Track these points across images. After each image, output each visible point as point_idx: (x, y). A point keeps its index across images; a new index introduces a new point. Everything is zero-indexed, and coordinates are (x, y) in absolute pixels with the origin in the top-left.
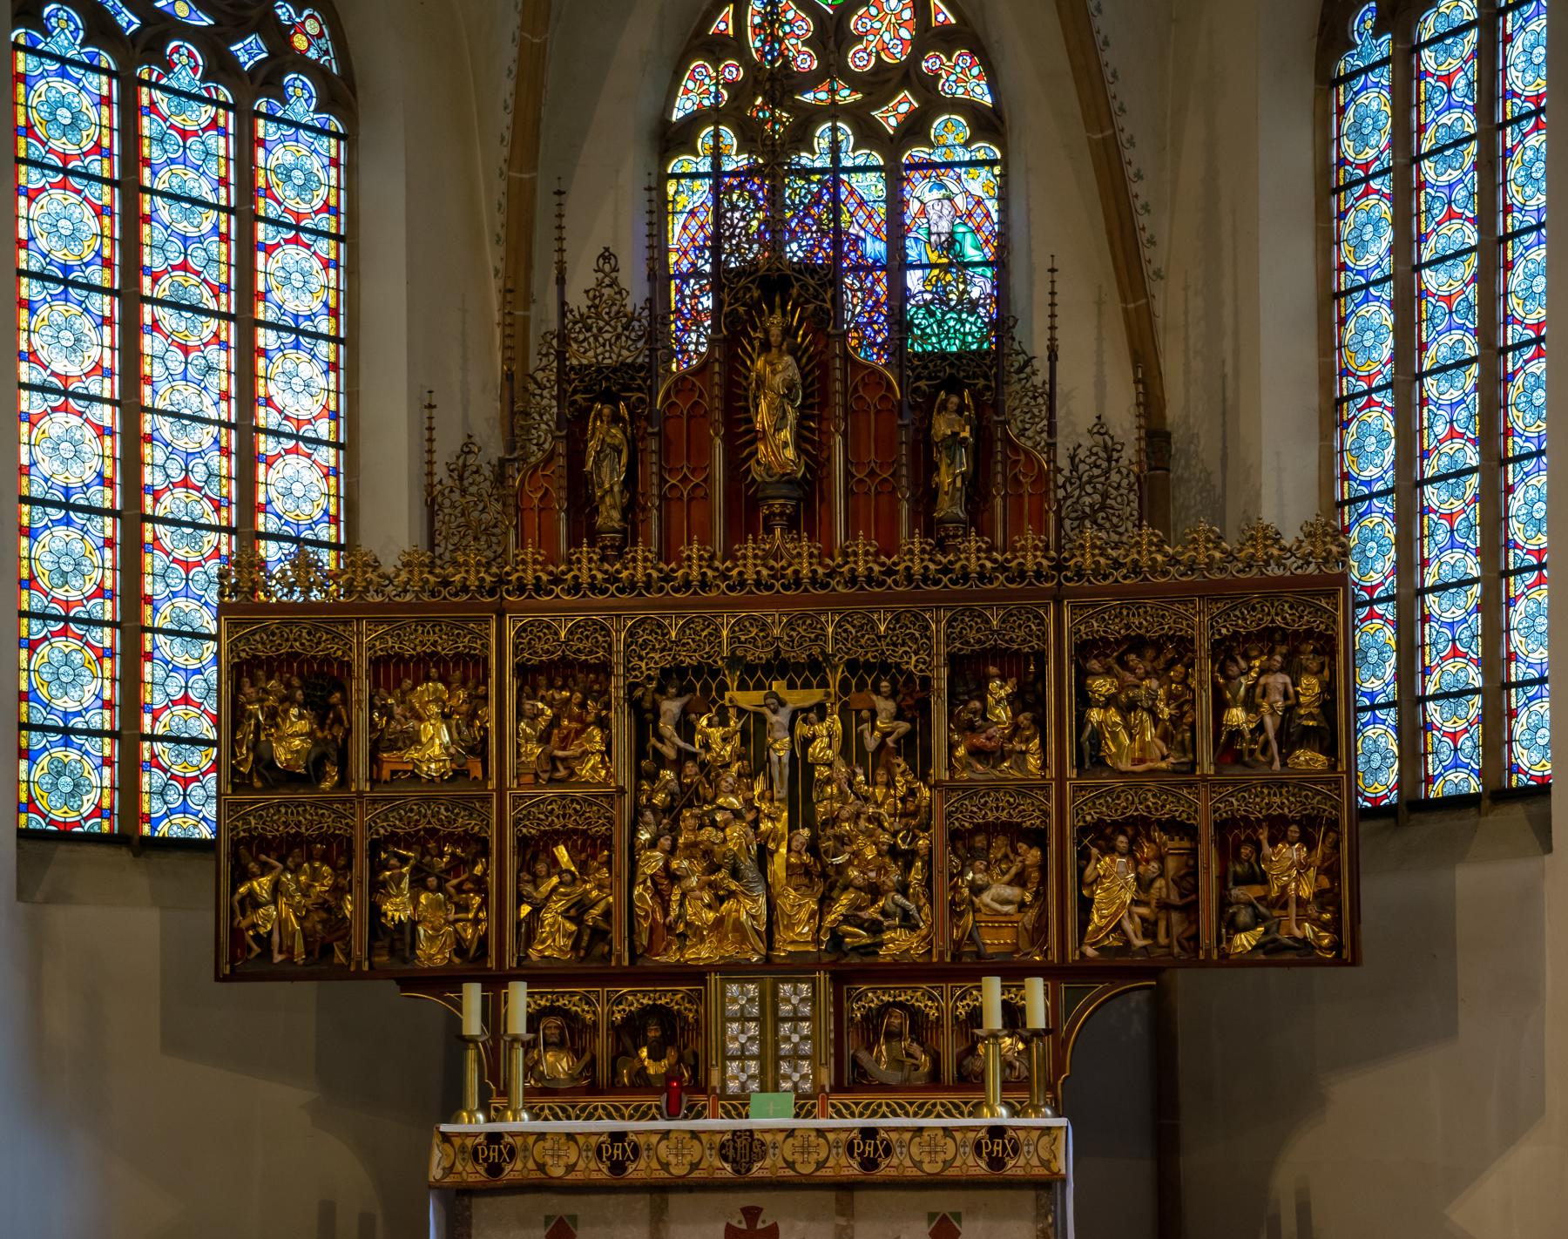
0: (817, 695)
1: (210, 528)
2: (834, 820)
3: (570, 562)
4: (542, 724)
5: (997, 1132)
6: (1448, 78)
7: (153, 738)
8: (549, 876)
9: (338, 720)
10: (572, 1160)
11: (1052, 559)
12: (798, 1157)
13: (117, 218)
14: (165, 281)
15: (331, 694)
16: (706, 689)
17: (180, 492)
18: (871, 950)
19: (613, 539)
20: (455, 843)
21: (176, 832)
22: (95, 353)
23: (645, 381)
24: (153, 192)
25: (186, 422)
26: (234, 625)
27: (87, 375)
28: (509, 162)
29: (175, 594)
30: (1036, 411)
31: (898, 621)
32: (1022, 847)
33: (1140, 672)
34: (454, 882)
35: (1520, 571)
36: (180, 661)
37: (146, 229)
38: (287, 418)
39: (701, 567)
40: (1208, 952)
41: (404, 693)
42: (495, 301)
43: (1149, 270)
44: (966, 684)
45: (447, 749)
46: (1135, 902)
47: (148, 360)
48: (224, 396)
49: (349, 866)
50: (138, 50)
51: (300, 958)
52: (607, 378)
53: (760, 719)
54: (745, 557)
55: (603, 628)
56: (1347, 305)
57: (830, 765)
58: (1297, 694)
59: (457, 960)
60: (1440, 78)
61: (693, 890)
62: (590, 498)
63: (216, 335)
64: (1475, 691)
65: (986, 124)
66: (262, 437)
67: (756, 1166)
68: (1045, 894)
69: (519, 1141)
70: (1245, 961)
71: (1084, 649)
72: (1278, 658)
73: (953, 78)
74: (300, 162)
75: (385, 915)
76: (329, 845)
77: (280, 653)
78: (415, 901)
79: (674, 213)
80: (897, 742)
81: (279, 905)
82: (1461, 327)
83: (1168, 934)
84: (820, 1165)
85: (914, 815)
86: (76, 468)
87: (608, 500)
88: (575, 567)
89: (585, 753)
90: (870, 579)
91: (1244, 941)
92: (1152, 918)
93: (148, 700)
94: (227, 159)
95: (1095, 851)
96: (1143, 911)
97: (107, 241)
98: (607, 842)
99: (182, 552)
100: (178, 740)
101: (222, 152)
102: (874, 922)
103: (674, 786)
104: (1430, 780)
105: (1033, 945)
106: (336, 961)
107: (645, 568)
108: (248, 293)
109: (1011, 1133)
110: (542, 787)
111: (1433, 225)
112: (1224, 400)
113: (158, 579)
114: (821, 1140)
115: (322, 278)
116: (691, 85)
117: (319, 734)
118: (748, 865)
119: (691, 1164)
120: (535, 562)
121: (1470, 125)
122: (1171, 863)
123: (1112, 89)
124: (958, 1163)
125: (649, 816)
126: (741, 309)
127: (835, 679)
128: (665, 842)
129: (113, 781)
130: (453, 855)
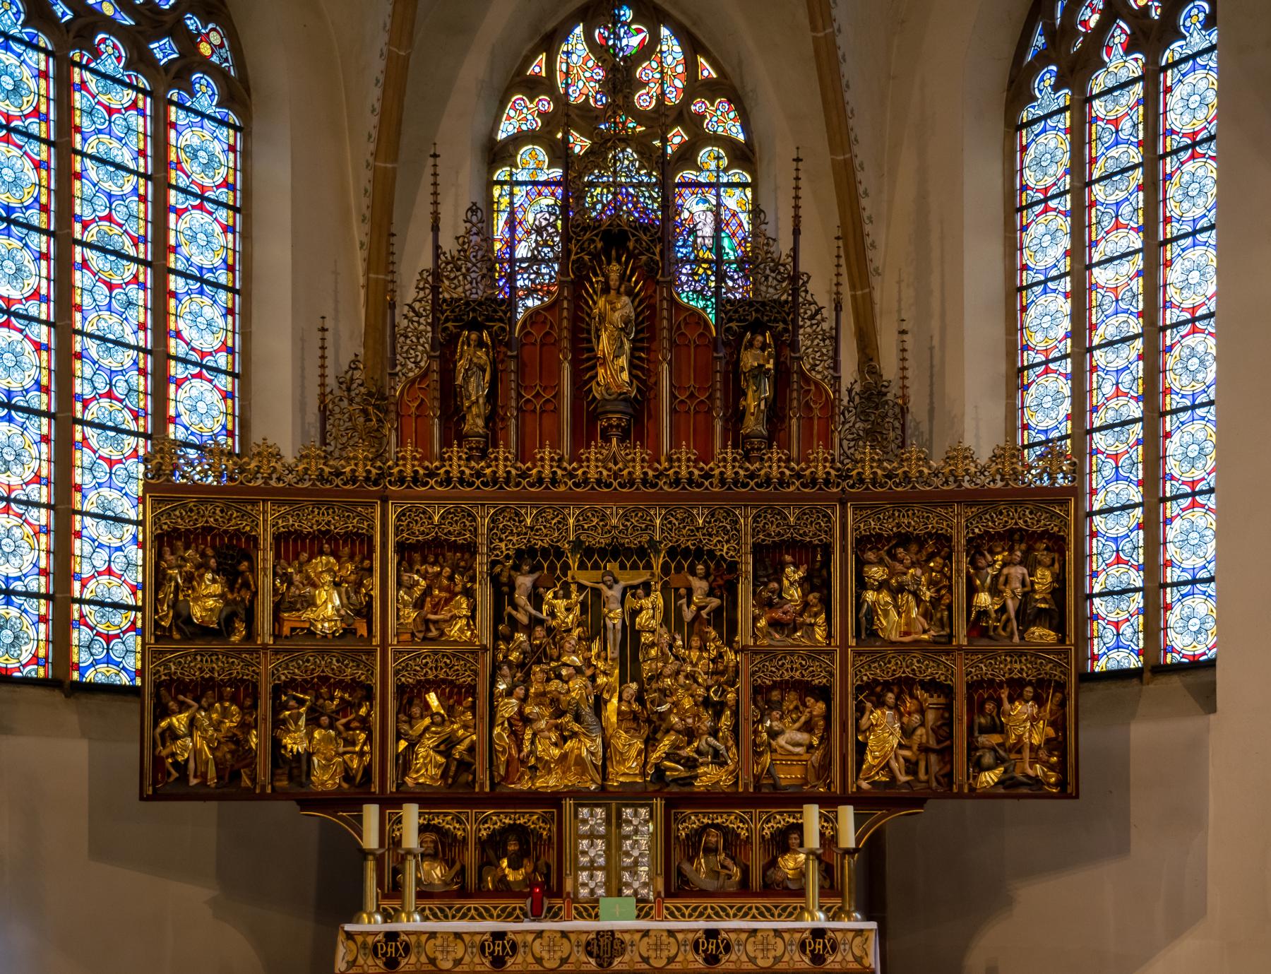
0: (644, 576)
1: (129, 433)
2: (658, 676)
3: (442, 459)
4: (417, 592)
5: (818, 933)
6: (1116, 122)
7: (81, 601)
8: (422, 717)
9: (246, 585)
10: (459, 955)
11: (838, 470)
12: (652, 954)
13: (53, 172)
14: (93, 229)
15: (239, 563)
16: (552, 568)
17: (105, 402)
18: (688, 781)
19: (478, 442)
20: (344, 690)
21: (101, 679)
22: (33, 281)
23: (505, 313)
24: (83, 155)
25: (110, 345)
26: (157, 501)
27: (27, 299)
28: (375, 155)
29: (100, 485)
30: (824, 351)
31: (713, 516)
32: (810, 701)
33: (908, 562)
34: (344, 721)
35: (1175, 498)
36: (104, 540)
37: (77, 184)
38: (193, 349)
39: (552, 467)
40: (961, 787)
41: (301, 564)
42: (360, 267)
43: (871, 267)
44: (766, 569)
45: (338, 611)
46: (900, 746)
47: (79, 291)
48: (142, 327)
49: (255, 706)
50: (71, 35)
51: (212, 782)
52: (474, 310)
53: (597, 593)
54: (588, 460)
55: (469, 515)
56: (1028, 296)
57: (653, 632)
58: (1032, 583)
59: (345, 786)
60: (1108, 122)
61: (542, 731)
62: (458, 409)
63: (136, 277)
64: (1136, 590)
65: (742, 155)
66: (173, 363)
67: (617, 961)
68: (829, 739)
69: (413, 939)
70: (988, 795)
71: (863, 543)
72: (1019, 553)
73: (715, 119)
74: (203, 145)
75: (285, 747)
76: (237, 688)
77: (196, 525)
78: (310, 736)
79: (498, 211)
80: (708, 614)
81: (195, 737)
82: (1126, 311)
83: (927, 772)
84: (671, 960)
85: (722, 673)
86: (17, 375)
87: (474, 410)
88: (447, 463)
89: (454, 617)
90: (690, 481)
91: (989, 778)
92: (914, 759)
93: (77, 570)
94: (145, 135)
95: (869, 705)
96: (907, 753)
97: (44, 190)
98: (471, 690)
99: (107, 451)
100: (102, 604)
101: (141, 129)
102: (688, 758)
103: (526, 645)
104: (1096, 658)
105: (818, 779)
106: (243, 784)
107: (506, 466)
108: (162, 247)
109: (830, 934)
110: (418, 644)
111: (1103, 234)
112: (932, 366)
113: (87, 472)
114: (672, 940)
115: (222, 240)
116: (512, 113)
117: (229, 596)
118: (587, 710)
119: (562, 959)
120: (414, 458)
121: (1136, 156)
122: (931, 716)
123: (851, 122)
124: (786, 958)
125: (505, 669)
126: (586, 258)
127: (657, 562)
128: (520, 691)
129: (47, 636)
130: (342, 698)
